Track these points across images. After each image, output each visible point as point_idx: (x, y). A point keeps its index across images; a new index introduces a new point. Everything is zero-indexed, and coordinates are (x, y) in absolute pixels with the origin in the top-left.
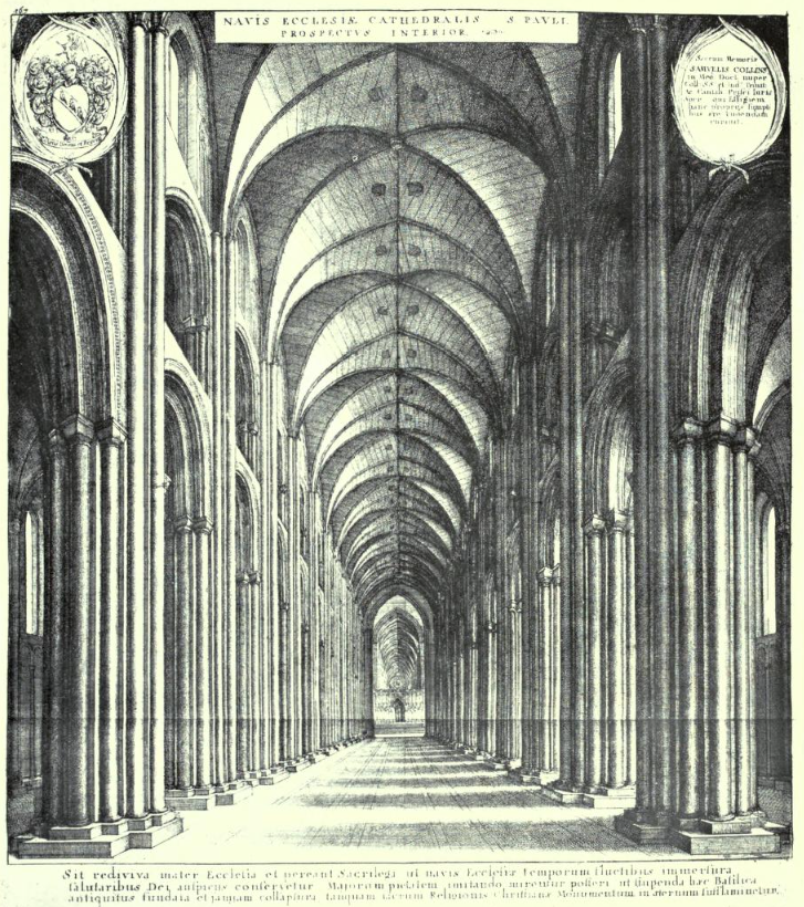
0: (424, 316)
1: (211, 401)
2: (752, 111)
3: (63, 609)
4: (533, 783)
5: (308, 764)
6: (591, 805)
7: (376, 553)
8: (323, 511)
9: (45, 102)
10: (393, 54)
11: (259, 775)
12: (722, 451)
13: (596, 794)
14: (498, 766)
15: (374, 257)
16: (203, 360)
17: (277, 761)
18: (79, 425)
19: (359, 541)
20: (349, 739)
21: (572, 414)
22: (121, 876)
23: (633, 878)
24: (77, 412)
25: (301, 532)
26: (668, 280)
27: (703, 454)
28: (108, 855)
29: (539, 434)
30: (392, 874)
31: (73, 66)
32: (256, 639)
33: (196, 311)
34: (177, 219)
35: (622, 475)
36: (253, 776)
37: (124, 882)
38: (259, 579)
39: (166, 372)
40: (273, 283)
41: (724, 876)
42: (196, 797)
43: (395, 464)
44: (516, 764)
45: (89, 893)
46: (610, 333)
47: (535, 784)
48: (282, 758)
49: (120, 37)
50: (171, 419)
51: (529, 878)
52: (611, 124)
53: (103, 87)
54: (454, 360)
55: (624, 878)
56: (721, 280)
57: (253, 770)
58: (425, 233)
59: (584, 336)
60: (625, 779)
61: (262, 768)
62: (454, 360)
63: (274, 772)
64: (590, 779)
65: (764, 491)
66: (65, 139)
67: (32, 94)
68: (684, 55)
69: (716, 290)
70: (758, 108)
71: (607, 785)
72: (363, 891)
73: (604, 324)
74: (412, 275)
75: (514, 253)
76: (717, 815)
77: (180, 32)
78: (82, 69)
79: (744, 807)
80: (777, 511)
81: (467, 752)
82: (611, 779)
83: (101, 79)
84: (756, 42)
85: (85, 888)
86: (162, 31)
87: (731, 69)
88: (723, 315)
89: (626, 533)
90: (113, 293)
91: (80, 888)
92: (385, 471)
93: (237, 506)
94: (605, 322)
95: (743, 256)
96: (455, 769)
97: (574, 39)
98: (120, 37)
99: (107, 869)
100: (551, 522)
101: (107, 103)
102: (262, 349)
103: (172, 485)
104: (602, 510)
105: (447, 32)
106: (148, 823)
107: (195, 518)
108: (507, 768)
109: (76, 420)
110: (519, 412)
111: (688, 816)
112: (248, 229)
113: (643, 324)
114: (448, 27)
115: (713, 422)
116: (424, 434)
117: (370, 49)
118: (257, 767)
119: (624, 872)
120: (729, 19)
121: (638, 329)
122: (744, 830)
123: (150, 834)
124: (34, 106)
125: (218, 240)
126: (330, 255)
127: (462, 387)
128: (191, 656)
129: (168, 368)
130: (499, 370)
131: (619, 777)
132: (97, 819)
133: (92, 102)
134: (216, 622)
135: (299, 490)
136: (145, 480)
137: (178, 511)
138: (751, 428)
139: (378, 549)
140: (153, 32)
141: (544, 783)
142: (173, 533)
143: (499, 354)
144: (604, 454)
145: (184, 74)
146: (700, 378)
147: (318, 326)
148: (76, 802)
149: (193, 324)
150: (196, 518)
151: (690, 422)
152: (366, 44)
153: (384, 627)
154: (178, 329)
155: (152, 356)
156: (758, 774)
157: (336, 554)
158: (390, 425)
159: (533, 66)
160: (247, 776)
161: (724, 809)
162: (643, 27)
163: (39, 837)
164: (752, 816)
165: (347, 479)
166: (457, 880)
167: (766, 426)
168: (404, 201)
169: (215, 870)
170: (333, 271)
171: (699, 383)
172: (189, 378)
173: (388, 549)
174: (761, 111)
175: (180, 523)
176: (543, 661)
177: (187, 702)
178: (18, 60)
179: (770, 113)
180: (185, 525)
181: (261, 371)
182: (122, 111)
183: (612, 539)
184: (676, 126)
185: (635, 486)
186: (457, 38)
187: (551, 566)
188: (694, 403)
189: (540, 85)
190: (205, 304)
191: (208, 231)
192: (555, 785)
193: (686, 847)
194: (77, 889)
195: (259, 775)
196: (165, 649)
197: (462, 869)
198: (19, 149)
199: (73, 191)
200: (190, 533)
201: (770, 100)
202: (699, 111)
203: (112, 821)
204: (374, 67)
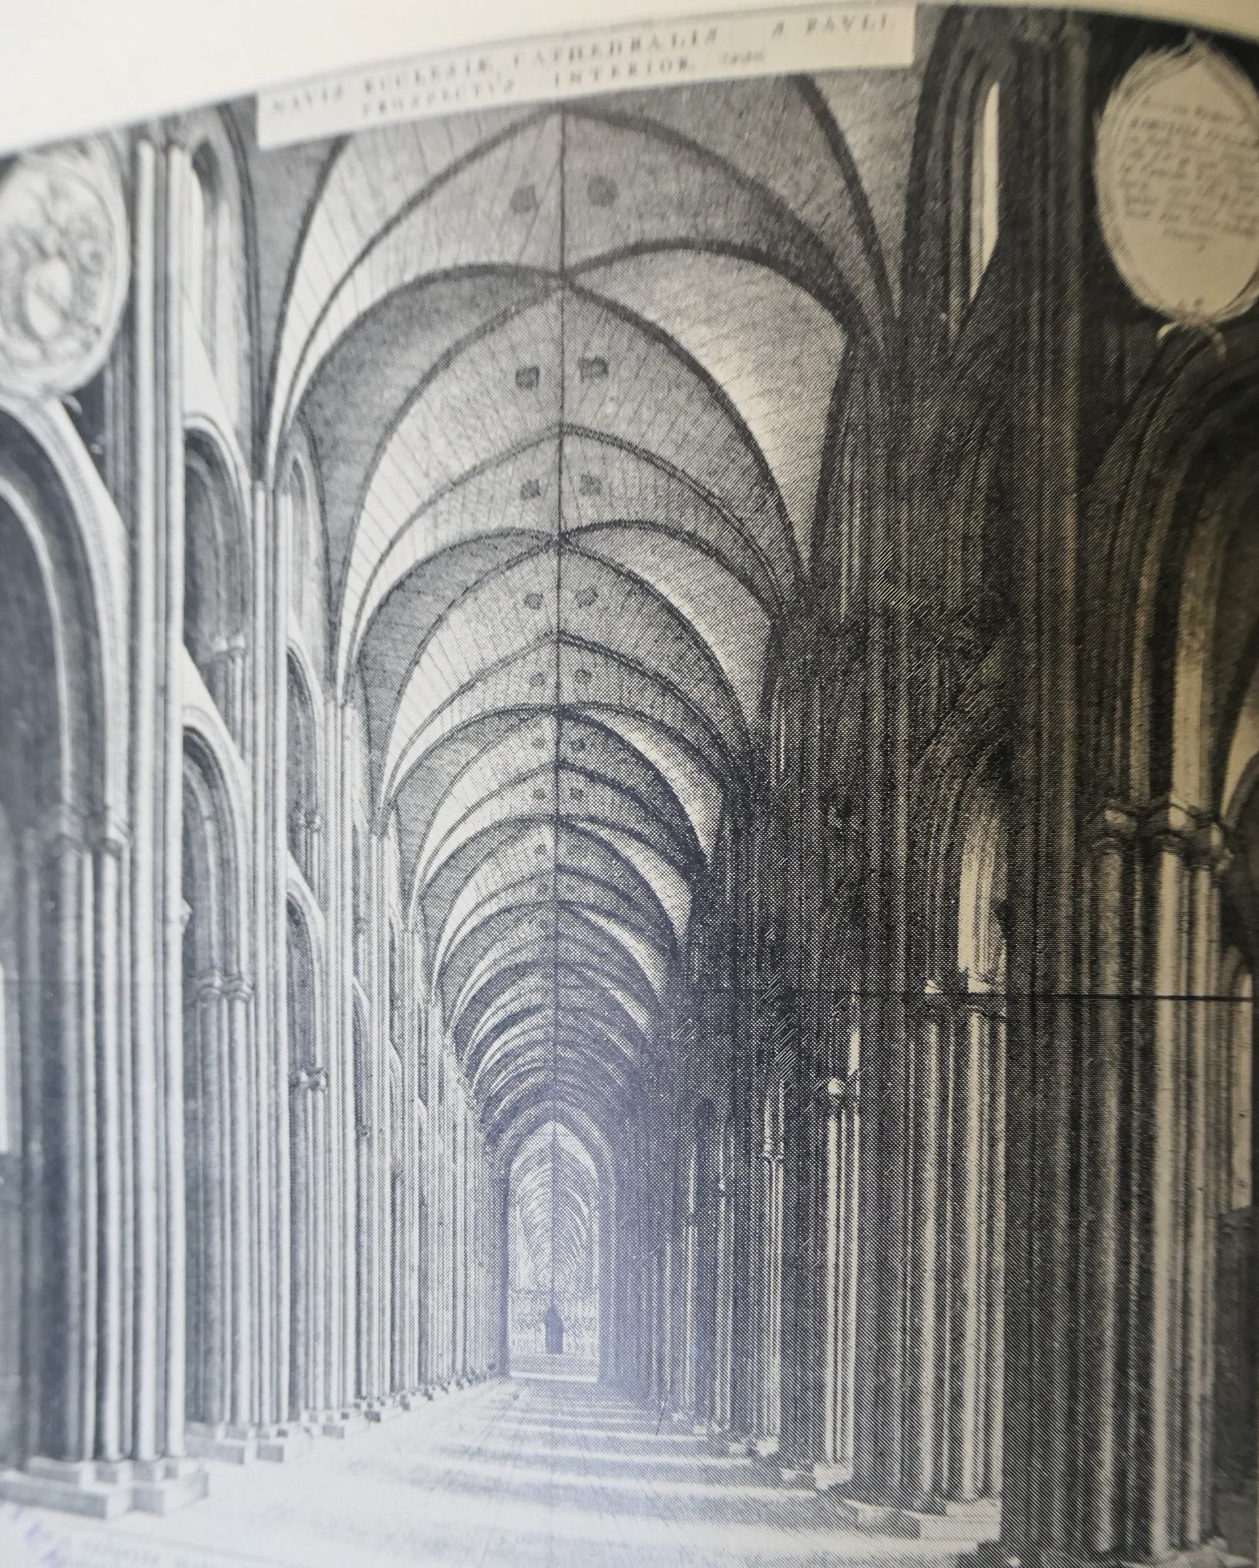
5: (400, 1409)
12: (1170, 863)
14: (734, 1447)
35: (984, 905)
57: (314, 1408)
60: (980, 1485)
63: (345, 1416)
102: (330, 677)
103: (192, 918)
126: (442, 505)
135: (387, 929)
144: (953, 857)
151: (1117, 809)
167: (1240, 823)
170: (448, 534)
175: (206, 981)
183: (963, 1030)
186: (674, 77)
192: (840, 1491)
204: (522, 146)
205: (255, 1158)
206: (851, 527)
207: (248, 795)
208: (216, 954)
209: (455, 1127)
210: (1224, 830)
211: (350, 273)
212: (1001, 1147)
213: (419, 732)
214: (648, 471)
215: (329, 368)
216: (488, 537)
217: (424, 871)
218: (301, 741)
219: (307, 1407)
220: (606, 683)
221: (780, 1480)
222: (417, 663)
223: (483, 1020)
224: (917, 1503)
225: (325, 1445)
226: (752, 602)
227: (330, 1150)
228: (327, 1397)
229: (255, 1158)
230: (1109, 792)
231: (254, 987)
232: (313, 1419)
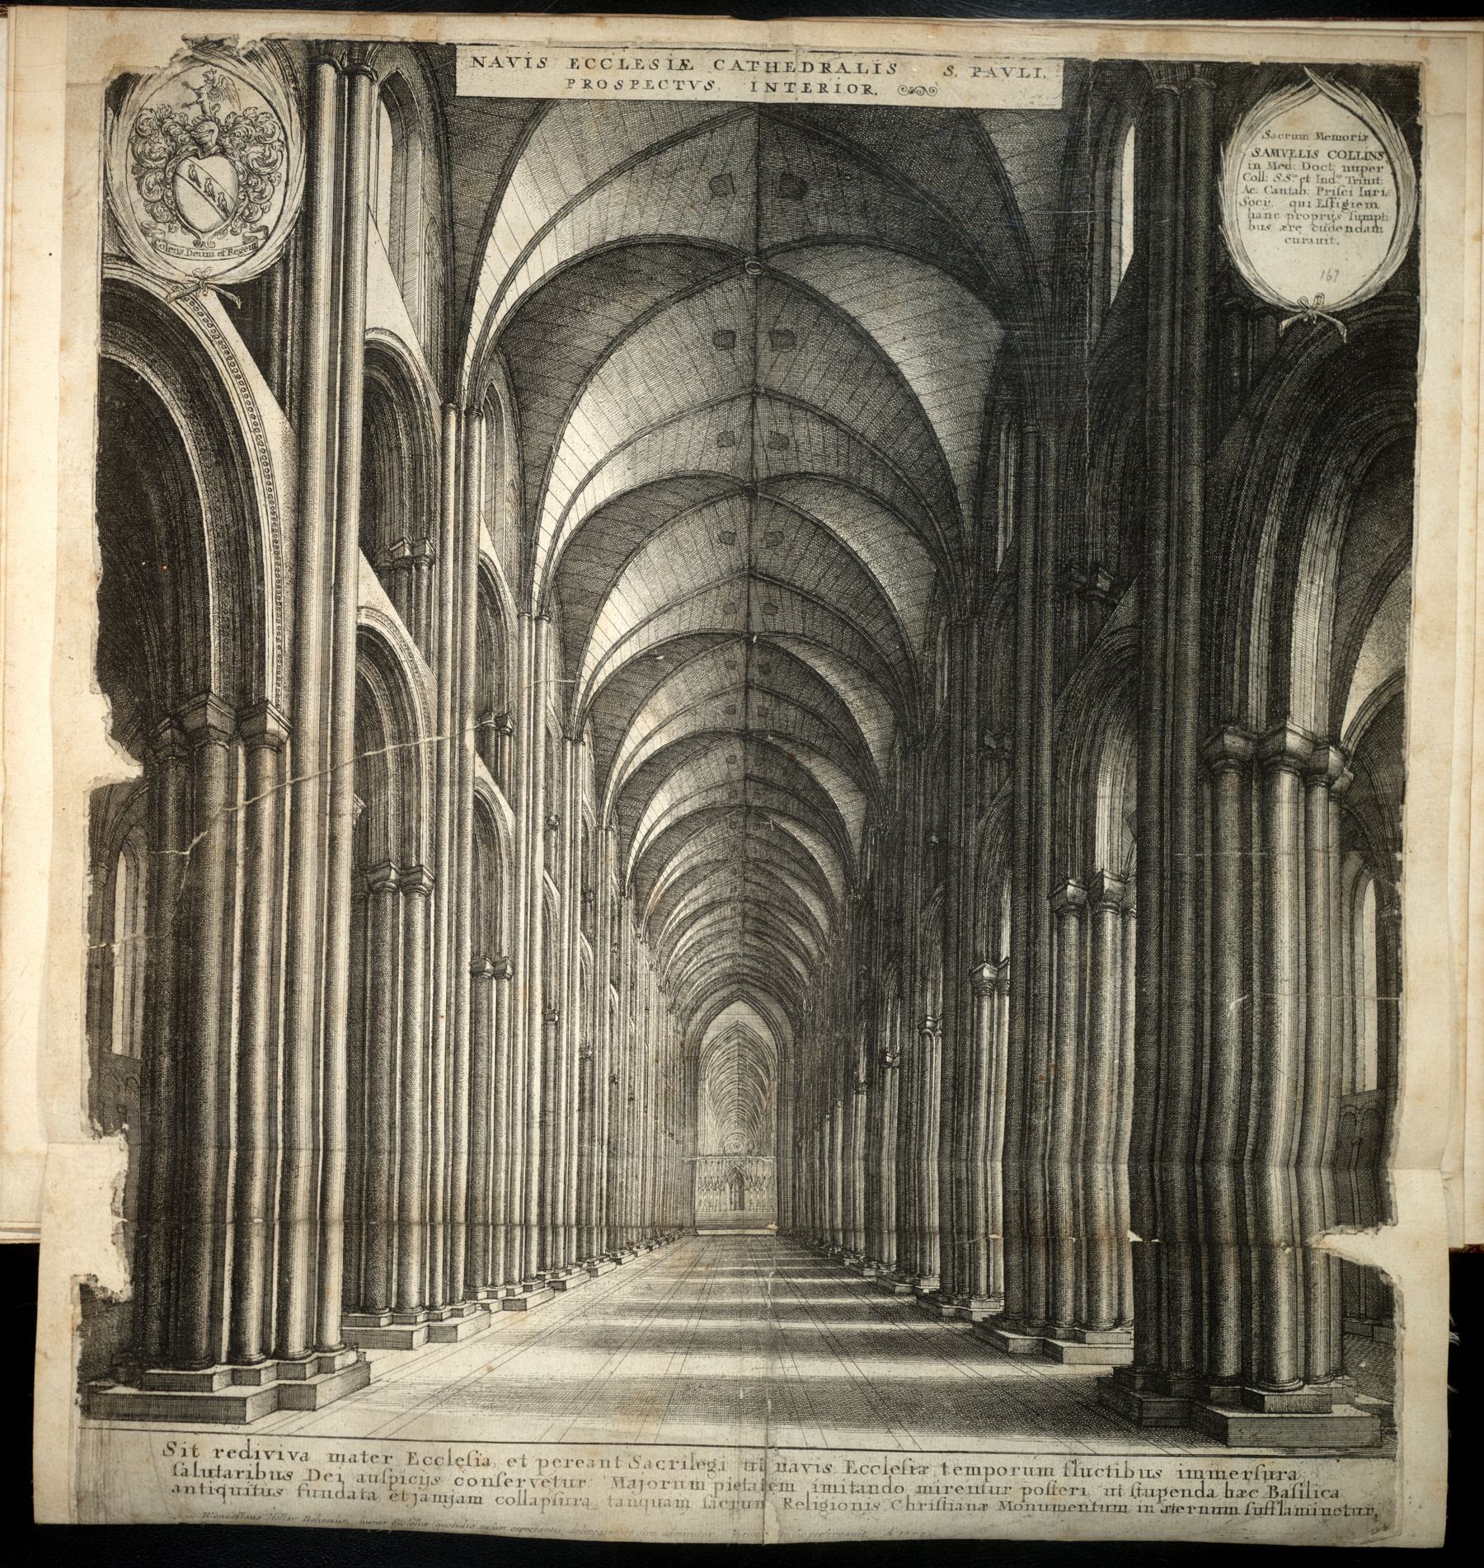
0: (792, 548)
1: (434, 677)
2: (1355, 224)
3: (175, 1017)
4: (958, 1317)
5: (587, 1277)
6: (1056, 1356)
7: (708, 931)
8: (621, 858)
10: (752, 121)
11: (502, 1294)
12: (1286, 783)
13: (1066, 1339)
15: (714, 448)
16: (423, 610)
17: (534, 1271)
18: (210, 711)
19: (681, 911)
21: (1036, 715)
22: (262, 1455)
23: (1127, 1484)
24: (208, 691)
25: (583, 894)
29: (980, 741)
31: (213, 126)
32: (504, 1069)
33: (413, 530)
34: (385, 381)
35: (1118, 816)
36: (492, 1295)
37: (266, 1465)
38: (509, 970)
39: (360, 628)
40: (543, 488)
41: (1284, 1485)
43: (740, 786)
44: (930, 1285)
45: (206, 1482)
46: (1103, 584)
47: (964, 1320)
48: (542, 1266)
49: (295, 80)
51: (952, 1480)
52: (1115, 242)
53: (262, 160)
54: (844, 621)
55: (1114, 1483)
56: (1293, 502)
57: (493, 1285)
58: (798, 413)
60: (1115, 1315)
61: (508, 1281)
62: (844, 621)
63: (527, 1289)
67: (140, 168)
69: (1285, 519)
71: (1085, 1324)
72: (672, 1494)
73: (1096, 566)
74: (774, 480)
75: (947, 449)
76: (1274, 1381)
77: (395, 77)
78: (226, 130)
79: (1320, 1370)
80: (1378, 885)
81: (847, 1262)
82: (1093, 1313)
83: (259, 149)
84: (1370, 110)
85: (199, 1473)
86: (366, 73)
87: (1323, 155)
89: (1123, 912)
90: (272, 500)
91: (191, 1471)
92: (726, 795)
93: (475, 849)
95: (1331, 462)
96: (829, 1291)
97: (1058, 104)
98: (295, 80)
99: (239, 1443)
100: (996, 891)
101: (269, 187)
103: (365, 812)
105: (843, 89)
106: (309, 1370)
108: (915, 1291)
109: (204, 705)
110: (948, 707)
111: (1223, 1381)
112: (503, 401)
114: (845, 80)
115: (1274, 733)
116: (788, 738)
117: (713, 112)
118: (501, 1279)
119: (1113, 1473)
120: (1323, 69)
121: (1151, 580)
123: (314, 1387)
124: (144, 188)
125: (453, 416)
126: (640, 446)
128: (392, 1095)
129: (364, 621)
131: (1105, 1311)
132: (224, 1360)
133: (243, 186)
135: (580, 825)
136: (322, 805)
137: (375, 856)
139: (709, 926)
140: (350, 75)
142: (366, 897)
143: (915, 613)
144: (1088, 778)
145: (401, 145)
148: (190, 1328)
149: (408, 553)
150: (405, 869)
151: (1235, 733)
152: (707, 103)
153: (718, 1053)
154: (384, 561)
155: (338, 601)
156: (1344, 1315)
157: (641, 931)
158: (737, 722)
160: (482, 1295)
161: (1285, 1368)
162: (1174, 82)
165: (658, 812)
166: (824, 1478)
167: (1361, 746)
169: (422, 1450)
170: (647, 471)
173: (726, 926)
175: (379, 875)
176: (976, 1118)
177: (385, 1168)
178: (117, 112)
179: (1388, 227)
180: (387, 878)
181: (520, 630)
182: (296, 201)
183: (1098, 922)
184: (1225, 246)
185: (1140, 836)
187: (995, 961)
188: (1244, 702)
189: (996, 177)
190: (429, 521)
191: (435, 401)
192: (995, 1321)
193: (1218, 1433)
194: (186, 1473)
195: (502, 1294)
197: (838, 1461)
198: (118, 258)
199: (208, 330)
200: (395, 892)
201: (1387, 205)
202: (1266, 223)
203: (250, 1363)
204: (719, 140)
207: (432, 698)
209: (647, 1009)
210: (1345, 755)
212: (1131, 1025)
213: (616, 646)
214: (830, 431)
215: (529, 307)
216: (685, 477)
217: (618, 774)
218: (492, 649)
219: (485, 1285)
222: (615, 585)
224: (1060, 1331)
225: (501, 1319)
226: (921, 550)
229: (430, 1045)
230: (1230, 721)
231: (436, 881)
232: (492, 1295)
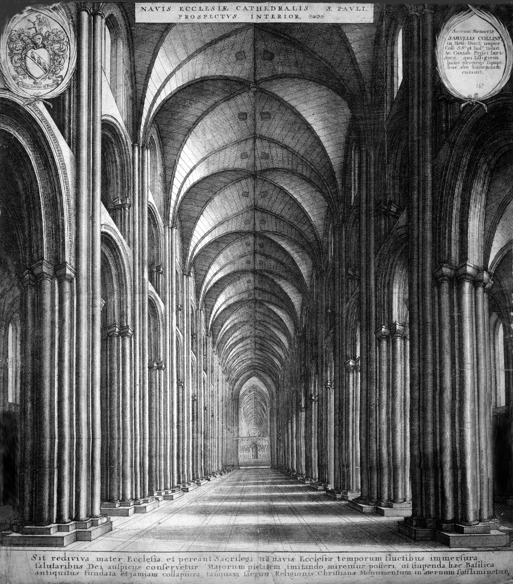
0: (271, 198)
1: (132, 251)
2: (490, 65)
3: (33, 387)
4: (343, 499)
5: (196, 486)
7: (241, 349)
8: (207, 321)
9: (21, 59)
10: (252, 30)
12: (467, 286)
14: (320, 488)
15: (240, 159)
17: (176, 484)
18: (44, 267)
20: (223, 470)
23: (410, 563)
25: (192, 335)
26: (433, 175)
27: (455, 287)
28: (62, 545)
30: (250, 559)
31: (40, 36)
33: (122, 194)
34: (110, 135)
35: (401, 300)
36: (159, 494)
37: (72, 563)
38: (163, 366)
39: (102, 233)
40: (173, 176)
41: (472, 562)
42: (121, 508)
45: (49, 570)
46: (394, 209)
47: (345, 500)
48: (179, 482)
49: (72, 18)
50: (106, 264)
51: (341, 563)
52: (395, 75)
53: (60, 49)
55: (405, 563)
56: (467, 175)
57: (160, 490)
58: (272, 145)
59: (376, 211)
61: (166, 489)
63: (173, 491)
64: (381, 497)
65: (495, 311)
66: (34, 83)
68: (445, 30)
70: (493, 63)
71: (393, 501)
72: (232, 571)
77: (111, 16)
81: (299, 478)
82: (396, 496)
83: (58, 45)
85: (46, 566)
86: (100, 14)
88: (469, 198)
89: (404, 338)
90: (67, 183)
91: (43, 566)
93: (149, 319)
94: (391, 202)
95: (482, 159)
97: (372, 21)
98: (72, 18)
99: (61, 555)
101: (63, 60)
102: (166, 218)
103: (106, 305)
104: (388, 322)
105: (287, 17)
106: (88, 525)
107: (121, 326)
108: (325, 489)
110: (334, 259)
111: (447, 522)
113: (416, 204)
114: (288, 13)
115: (462, 267)
116: (271, 273)
117: (236, 27)
118: (163, 488)
119: (405, 559)
121: (412, 207)
122: (486, 531)
123: (90, 532)
124: (13, 61)
125: (137, 149)
126: (211, 159)
127: (296, 243)
129: (103, 230)
130: (321, 233)
132: (55, 522)
133: (53, 60)
134: (135, 394)
135: (190, 309)
137: (110, 323)
138: (487, 272)
141: (350, 499)
143: (320, 222)
144: (389, 286)
145: (114, 42)
146: (453, 237)
147: (202, 204)
149: (120, 203)
150: (122, 327)
151: (447, 267)
153: (246, 397)
155: (93, 222)
159: (345, 41)
161: (471, 517)
162: (417, 11)
163: (16, 532)
164: (490, 522)
166: (292, 563)
167: (496, 271)
168: (259, 125)
170: (213, 169)
171: (453, 242)
172: (117, 235)
174: (496, 65)
175: (111, 330)
177: (116, 445)
179: (502, 67)
180: (115, 331)
181: (165, 232)
182: (73, 65)
183: (394, 343)
184: (438, 75)
185: (410, 308)
186: (293, 20)
187: (354, 358)
188: (450, 255)
189: (348, 50)
190: (128, 190)
191: (130, 143)
192: (357, 500)
194: (41, 567)
195: (163, 494)
196: (101, 412)
197: (297, 556)
199: (40, 117)
200: (118, 336)
202: (454, 66)
203: (65, 523)
204: (239, 38)
205: (133, 396)
206: (355, 174)
208: (117, 318)
211: (174, 72)
213: (203, 238)
214: (285, 152)
219: (157, 490)
220: (271, 225)
221: (336, 498)
223: (228, 342)
224: (383, 504)
225: (163, 503)
227: (166, 392)
228: (166, 484)
230: (445, 262)
232: (159, 494)
